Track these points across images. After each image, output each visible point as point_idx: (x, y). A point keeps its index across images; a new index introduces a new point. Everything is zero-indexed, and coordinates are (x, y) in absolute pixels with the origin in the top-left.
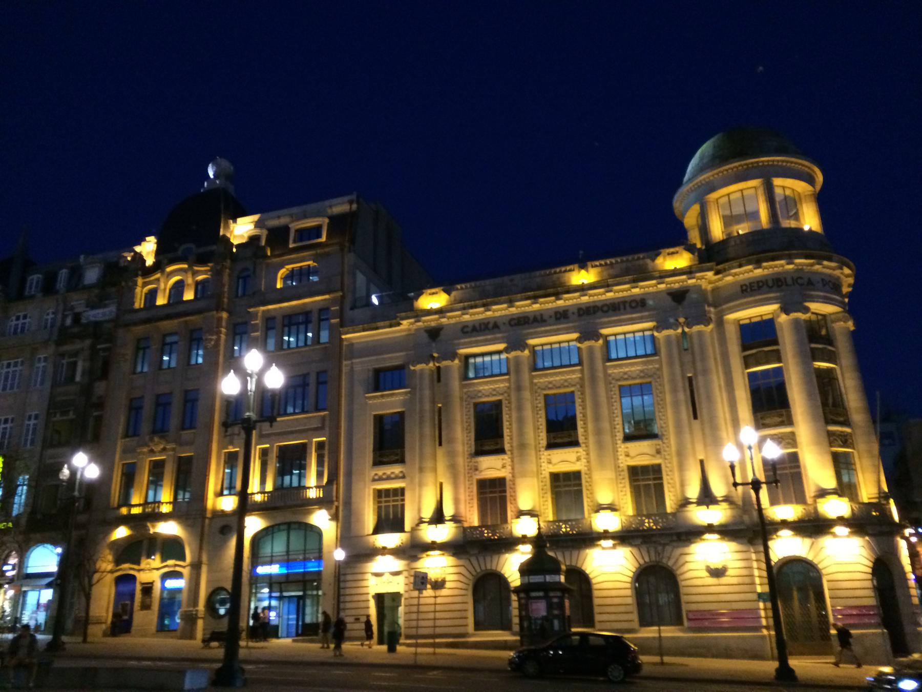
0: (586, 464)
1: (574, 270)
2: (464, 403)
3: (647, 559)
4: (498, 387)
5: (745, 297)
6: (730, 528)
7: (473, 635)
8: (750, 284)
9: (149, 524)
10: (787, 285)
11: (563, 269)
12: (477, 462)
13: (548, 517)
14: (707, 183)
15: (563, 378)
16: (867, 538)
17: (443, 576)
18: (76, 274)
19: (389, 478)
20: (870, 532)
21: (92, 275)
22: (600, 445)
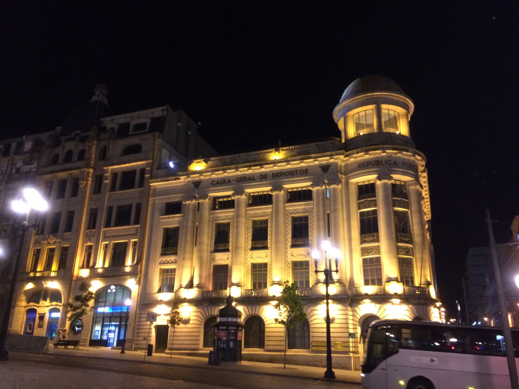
0: (270, 259)
1: (272, 152)
2: (211, 223)
3: (251, 313)
4: (229, 215)
5: (360, 170)
6: (339, 297)
7: (202, 350)
8: (363, 163)
9: (43, 282)
10: (382, 164)
11: (267, 151)
12: (214, 256)
13: (248, 287)
14: (348, 106)
15: (263, 211)
16: (411, 306)
17: (189, 317)
18: (21, 145)
19: (168, 263)
20: (412, 303)
21: (28, 146)
22: (277, 249)
